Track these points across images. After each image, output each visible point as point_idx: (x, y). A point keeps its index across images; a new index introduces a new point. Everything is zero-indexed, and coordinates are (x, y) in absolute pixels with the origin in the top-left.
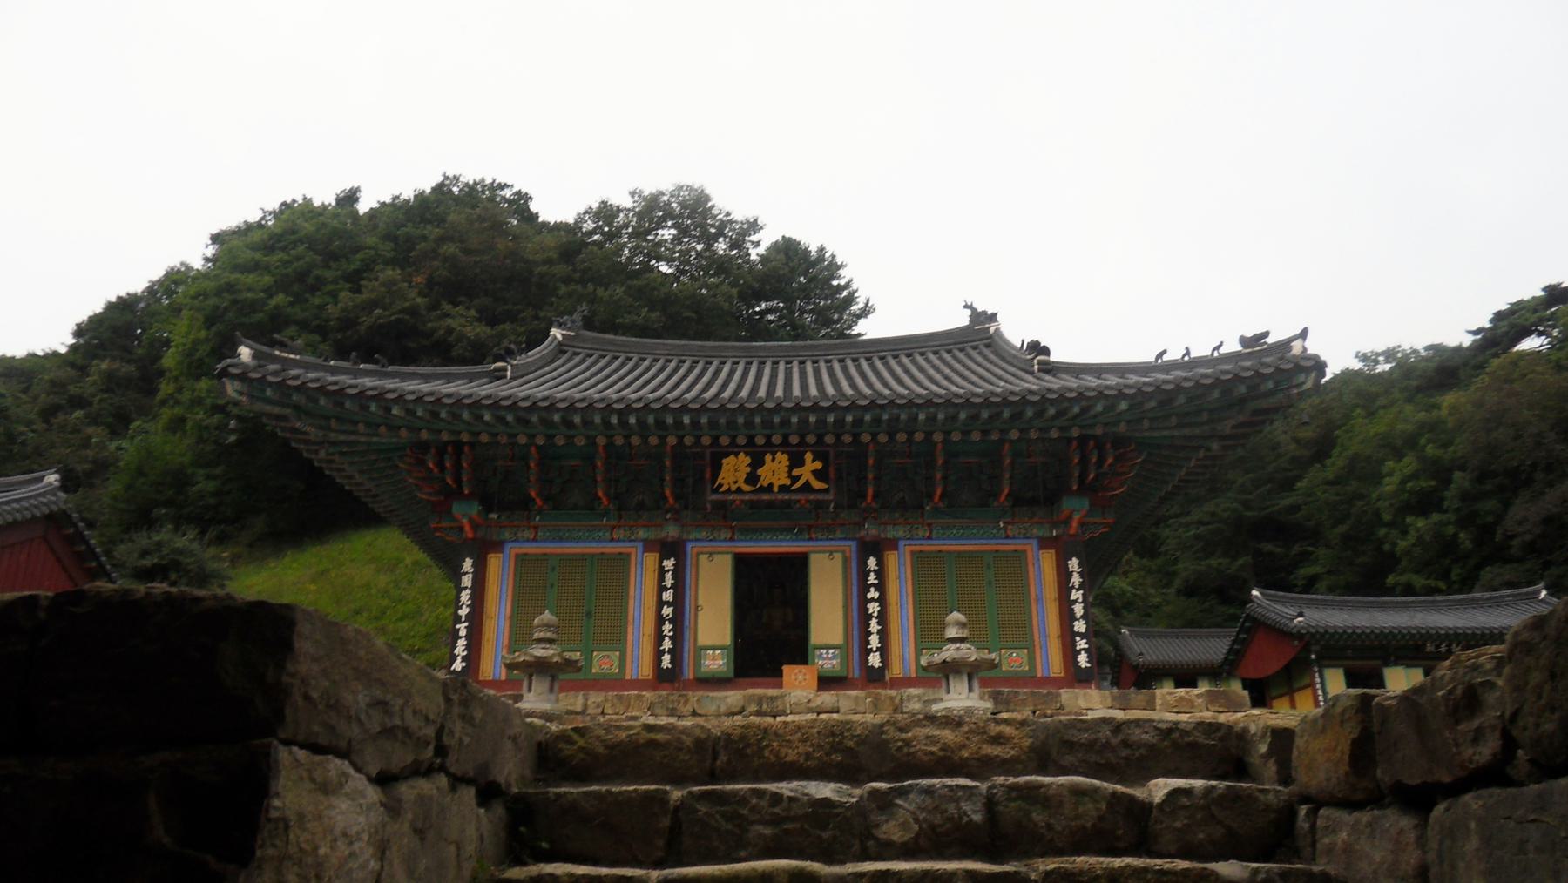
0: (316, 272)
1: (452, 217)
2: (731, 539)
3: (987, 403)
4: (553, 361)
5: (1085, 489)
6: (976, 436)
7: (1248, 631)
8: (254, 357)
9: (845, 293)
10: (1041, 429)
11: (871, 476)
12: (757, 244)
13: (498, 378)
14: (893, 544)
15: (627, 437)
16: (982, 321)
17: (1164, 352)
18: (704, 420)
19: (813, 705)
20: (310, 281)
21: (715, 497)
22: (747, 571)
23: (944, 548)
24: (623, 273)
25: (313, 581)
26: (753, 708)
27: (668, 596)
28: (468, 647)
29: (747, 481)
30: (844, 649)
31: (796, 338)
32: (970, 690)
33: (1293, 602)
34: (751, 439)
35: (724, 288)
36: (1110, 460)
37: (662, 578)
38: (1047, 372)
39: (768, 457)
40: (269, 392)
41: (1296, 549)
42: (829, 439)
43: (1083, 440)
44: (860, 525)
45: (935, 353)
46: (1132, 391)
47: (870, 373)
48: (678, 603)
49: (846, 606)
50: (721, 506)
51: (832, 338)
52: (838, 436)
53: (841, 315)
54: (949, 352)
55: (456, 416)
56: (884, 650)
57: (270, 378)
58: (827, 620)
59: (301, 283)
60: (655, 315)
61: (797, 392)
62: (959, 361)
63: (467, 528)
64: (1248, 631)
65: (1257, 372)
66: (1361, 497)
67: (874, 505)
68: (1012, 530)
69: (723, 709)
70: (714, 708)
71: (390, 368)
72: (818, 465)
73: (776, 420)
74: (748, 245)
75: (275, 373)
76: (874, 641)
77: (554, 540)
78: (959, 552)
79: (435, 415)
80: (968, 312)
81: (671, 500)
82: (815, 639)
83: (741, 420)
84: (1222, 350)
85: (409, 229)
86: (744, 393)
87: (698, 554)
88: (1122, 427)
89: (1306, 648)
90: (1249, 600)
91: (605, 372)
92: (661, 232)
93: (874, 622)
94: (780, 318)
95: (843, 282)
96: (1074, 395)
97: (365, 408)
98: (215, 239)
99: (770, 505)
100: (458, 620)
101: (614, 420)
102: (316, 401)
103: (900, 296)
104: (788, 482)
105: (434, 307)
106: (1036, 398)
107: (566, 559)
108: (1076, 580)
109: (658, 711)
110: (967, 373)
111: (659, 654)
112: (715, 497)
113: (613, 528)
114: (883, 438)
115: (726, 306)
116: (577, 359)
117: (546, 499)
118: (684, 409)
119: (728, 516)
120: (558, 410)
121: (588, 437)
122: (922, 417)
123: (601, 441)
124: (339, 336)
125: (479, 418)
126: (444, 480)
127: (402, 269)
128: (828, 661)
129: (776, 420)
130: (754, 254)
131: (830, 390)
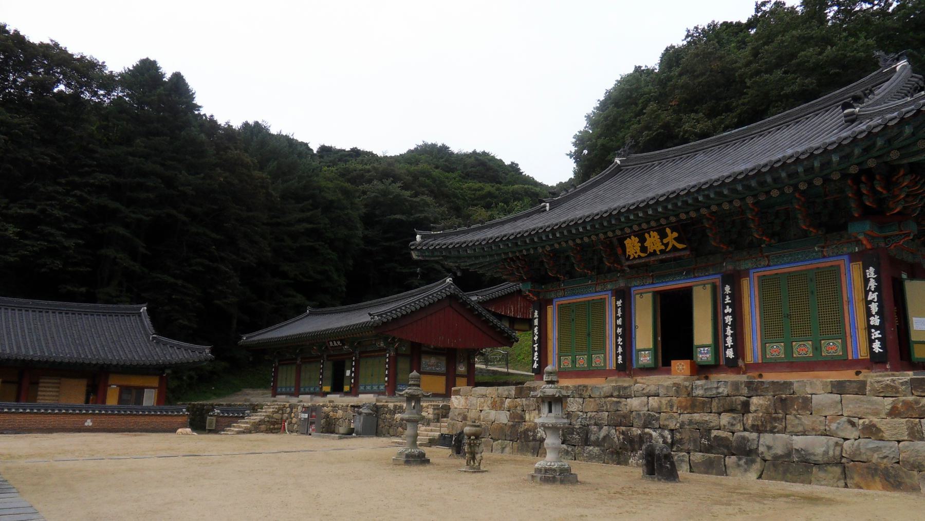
2: (653, 283)
5: (867, 213)
14: (746, 273)
21: (627, 263)
26: (615, 394)
27: (619, 322)
28: (539, 356)
32: (550, 411)
39: (647, 235)
72: (675, 235)
78: (789, 273)
82: (697, 341)
104: (663, 247)
112: (627, 263)
119: (647, 269)
127: (435, 197)
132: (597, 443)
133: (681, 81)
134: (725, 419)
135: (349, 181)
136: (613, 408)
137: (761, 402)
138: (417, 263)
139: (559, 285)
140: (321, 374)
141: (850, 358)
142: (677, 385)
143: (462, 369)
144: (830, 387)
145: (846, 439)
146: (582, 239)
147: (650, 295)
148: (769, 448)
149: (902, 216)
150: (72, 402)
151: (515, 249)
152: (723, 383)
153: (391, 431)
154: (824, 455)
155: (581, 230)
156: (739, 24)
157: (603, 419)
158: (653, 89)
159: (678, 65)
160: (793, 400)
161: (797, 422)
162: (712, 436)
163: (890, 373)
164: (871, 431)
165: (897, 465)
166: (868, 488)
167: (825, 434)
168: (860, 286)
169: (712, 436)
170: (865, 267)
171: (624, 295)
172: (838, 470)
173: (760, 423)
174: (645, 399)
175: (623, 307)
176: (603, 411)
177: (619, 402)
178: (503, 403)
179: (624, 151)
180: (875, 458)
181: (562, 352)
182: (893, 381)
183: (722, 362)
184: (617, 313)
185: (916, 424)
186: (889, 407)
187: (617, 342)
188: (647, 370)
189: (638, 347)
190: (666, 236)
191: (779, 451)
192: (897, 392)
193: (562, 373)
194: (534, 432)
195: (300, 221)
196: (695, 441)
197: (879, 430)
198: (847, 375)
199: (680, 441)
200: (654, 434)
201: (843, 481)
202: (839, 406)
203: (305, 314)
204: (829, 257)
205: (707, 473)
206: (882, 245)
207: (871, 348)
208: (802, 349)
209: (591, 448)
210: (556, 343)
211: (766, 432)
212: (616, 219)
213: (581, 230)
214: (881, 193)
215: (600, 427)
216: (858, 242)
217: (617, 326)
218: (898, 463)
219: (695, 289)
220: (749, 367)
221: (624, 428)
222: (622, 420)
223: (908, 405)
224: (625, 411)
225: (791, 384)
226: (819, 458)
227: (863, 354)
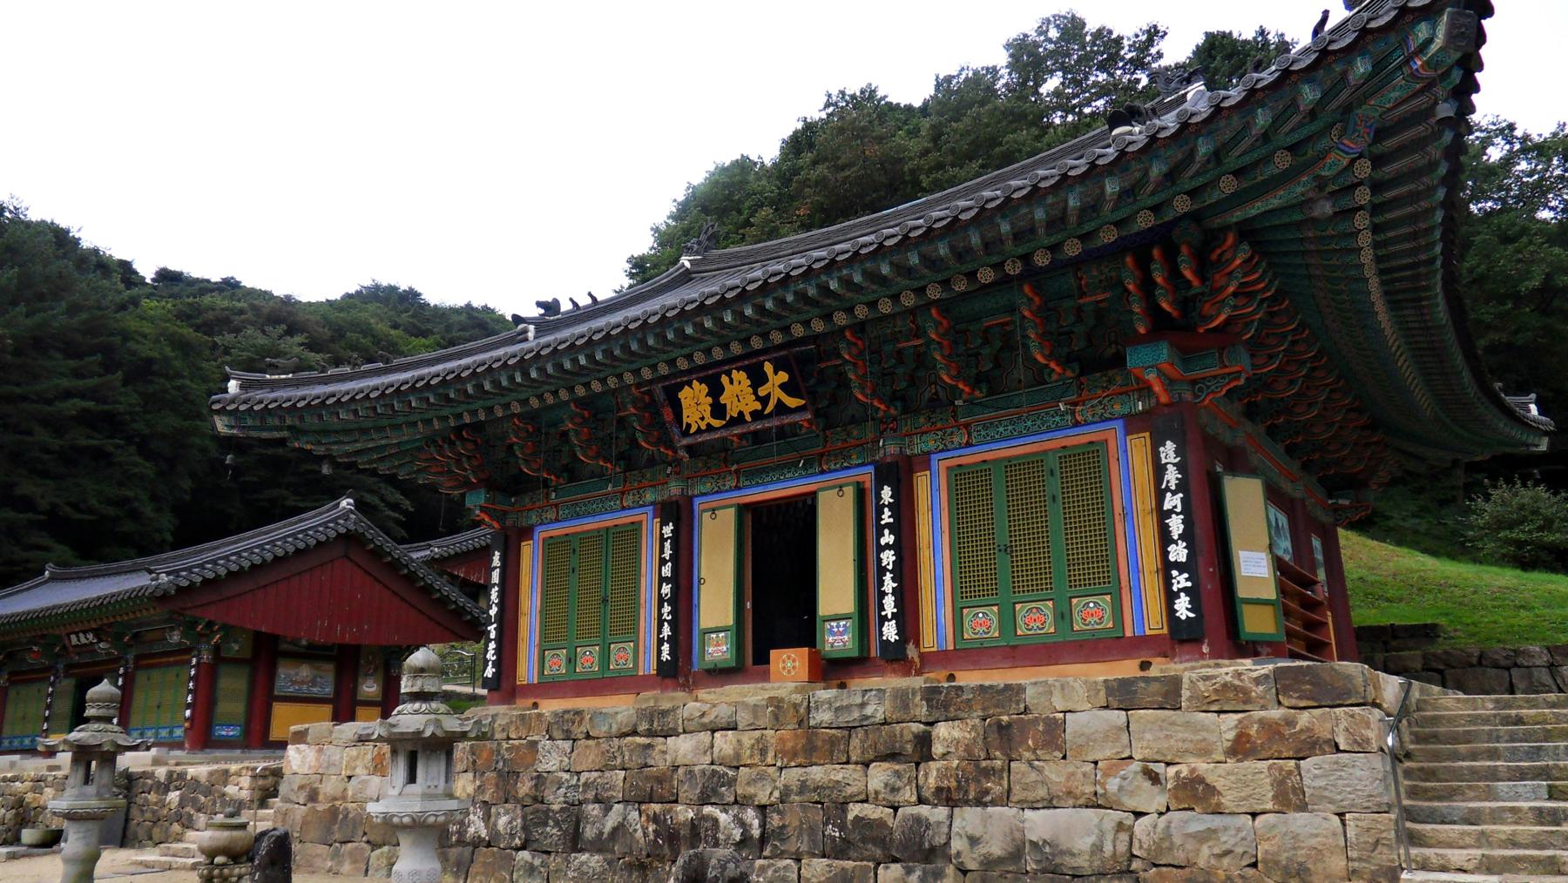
2: (737, 488)
5: (1161, 326)
14: (924, 461)
19: (706, 720)
21: (685, 442)
23: (556, 533)
26: (643, 727)
27: (667, 571)
28: (498, 651)
32: (412, 778)
39: (724, 379)
68: (1082, 412)
70: (604, 729)
72: (783, 377)
78: (1009, 459)
82: (823, 609)
104: (758, 406)
107: (585, 537)
109: (556, 734)
112: (685, 442)
117: (978, 381)
132: (598, 846)
133: (814, 175)
134: (879, 776)
135: (197, 328)
137: (956, 734)
138: (227, 443)
139: (547, 496)
140: (49, 707)
141: (1129, 633)
142: (776, 703)
143: (370, 688)
144: (1102, 694)
145: (1138, 815)
146: (587, 385)
147: (732, 511)
148: (974, 841)
149: (1225, 336)
151: (446, 412)
152: (873, 696)
153: (156, 832)
154: (1093, 853)
155: (583, 361)
156: (909, 108)
158: (771, 188)
159: (811, 146)
161: (1033, 776)
162: (850, 817)
163: (1212, 662)
164: (1195, 793)
165: (1251, 871)
167: (1095, 803)
168: (1144, 476)
169: (850, 817)
170: (1157, 444)
171: (679, 514)
173: (954, 784)
174: (705, 737)
175: (675, 539)
176: (614, 768)
177: (649, 746)
179: (699, 243)
180: (1204, 857)
181: (549, 639)
182: (1239, 675)
183: (875, 651)
184: (662, 551)
185: (1290, 773)
186: (1231, 735)
187: (660, 614)
188: (720, 674)
190: (764, 380)
191: (996, 849)
192: (1247, 701)
193: (548, 687)
194: (462, 823)
195: (68, 394)
196: (812, 830)
197: (1211, 790)
198: (1127, 669)
200: (723, 818)
202: (1125, 737)
203: (39, 580)
204: (1087, 424)
206: (1188, 396)
207: (1171, 611)
208: (1036, 619)
209: (584, 857)
211: (967, 803)
212: (656, 336)
213: (583, 361)
215: (606, 804)
216: (1145, 389)
217: (662, 580)
218: (1254, 865)
219: (821, 496)
220: (928, 660)
222: (652, 789)
223: (1272, 730)
225: (1021, 689)
227: (1155, 623)
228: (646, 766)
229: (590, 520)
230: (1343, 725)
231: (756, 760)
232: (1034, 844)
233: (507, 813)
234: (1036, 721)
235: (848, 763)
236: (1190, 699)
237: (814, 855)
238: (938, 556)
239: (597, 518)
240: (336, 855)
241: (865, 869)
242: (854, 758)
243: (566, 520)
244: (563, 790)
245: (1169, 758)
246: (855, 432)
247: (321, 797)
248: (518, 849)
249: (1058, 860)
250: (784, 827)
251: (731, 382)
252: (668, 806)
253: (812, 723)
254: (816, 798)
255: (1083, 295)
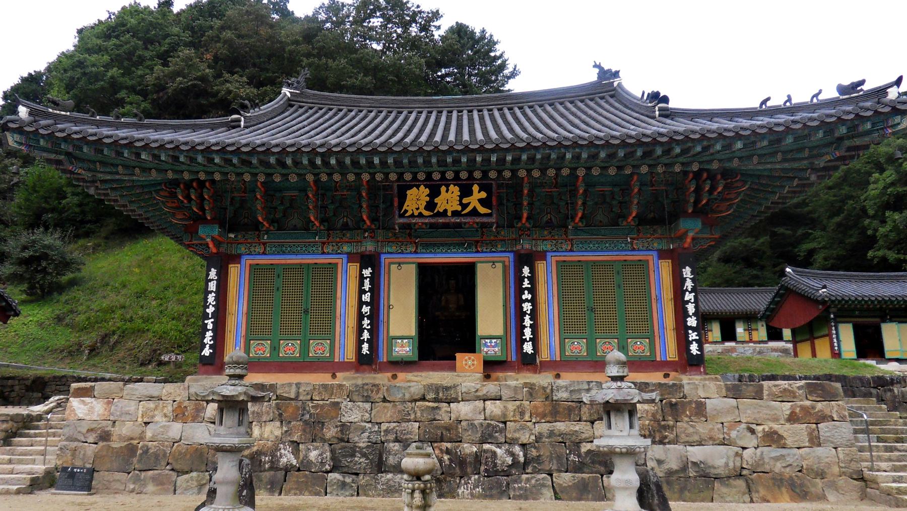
0: (139, 52)
1: (229, 13)
2: (416, 252)
3: (624, 144)
4: (283, 112)
5: (699, 212)
6: (612, 171)
7: (782, 296)
8: (30, 114)
9: (499, 62)
10: (666, 165)
11: (525, 203)
12: (439, 28)
13: (234, 127)
14: (542, 256)
15: (330, 175)
16: (607, 75)
17: (768, 99)
18: (390, 161)
19: (479, 394)
20: (135, 59)
21: (401, 220)
22: (428, 276)
24: (350, 48)
25: (139, 266)
26: (431, 396)
27: (366, 298)
28: (214, 338)
29: (426, 208)
30: (503, 339)
31: (466, 93)
32: (631, 427)
33: (815, 276)
34: (429, 176)
35: (416, 59)
36: (720, 189)
37: (362, 284)
38: (666, 116)
39: (443, 189)
40: (42, 142)
41: (800, 232)
42: (493, 175)
43: (697, 175)
44: (516, 240)
45: (571, 102)
46: (748, 133)
47: (523, 119)
48: (374, 304)
49: (505, 306)
50: (406, 227)
51: (491, 92)
52: (500, 172)
53: (497, 76)
54: (582, 101)
55: (193, 160)
56: (535, 340)
57: (41, 131)
58: (490, 317)
59: (128, 61)
60: (368, 79)
61: (466, 137)
62: (591, 109)
63: (211, 246)
64: (782, 296)
65: (857, 115)
66: (851, 197)
67: (528, 225)
68: (637, 244)
69: (407, 396)
71: (146, 121)
72: (483, 195)
73: (449, 160)
74: (433, 28)
75: (46, 127)
76: (528, 333)
77: (278, 254)
78: (594, 262)
79: (176, 159)
80: (597, 70)
81: (368, 222)
82: (482, 328)
83: (420, 160)
84: (821, 97)
85: (201, 22)
86: (423, 139)
87: (390, 264)
88: (735, 163)
89: (827, 311)
90: (783, 274)
91: (321, 121)
92: (372, 20)
93: (527, 318)
94: (455, 80)
95: (498, 54)
96: (697, 136)
97: (119, 154)
98: (80, 32)
99: (446, 226)
100: (206, 316)
101: (319, 161)
102: (81, 149)
103: (541, 60)
104: (459, 208)
105: (219, 75)
106: (665, 139)
107: (287, 268)
108: (689, 284)
109: (355, 398)
110: (600, 118)
111: (360, 343)
112: (401, 220)
113: (324, 243)
114: (536, 174)
115: (417, 71)
116: (301, 111)
117: (272, 222)
118: (374, 152)
119: (412, 235)
120: (274, 154)
121: (298, 175)
122: (569, 156)
123: (310, 178)
124: (155, 96)
125: (211, 160)
126: (190, 208)
127: (195, 48)
128: (491, 349)
129: (449, 160)
130: (437, 35)
131: (493, 134)
136: (427, 416)
144: (724, 390)
145: (744, 448)
148: (660, 462)
150: (646, 407)
157: (410, 433)
160: (684, 405)
161: (691, 430)
164: (773, 438)
166: (776, 500)
172: (741, 483)
174: (480, 404)
176: (409, 421)
178: (199, 410)
180: (778, 467)
186: (788, 412)
189: (392, 334)
191: (674, 465)
192: (795, 397)
194: (273, 455)
196: (559, 458)
197: (781, 437)
199: (538, 459)
200: (498, 451)
201: (747, 496)
202: (737, 411)
205: (580, 499)
209: (390, 476)
210: (243, 320)
214: (182, 202)
218: (800, 471)
221: (449, 445)
224: (447, 419)
226: (721, 471)
228: (435, 420)
229: (293, 257)
230: (835, 409)
231: (518, 418)
232: (694, 464)
233: (316, 448)
234: (690, 402)
235: (580, 421)
236: (768, 395)
237: (560, 471)
238: (551, 310)
239: (300, 257)
240: (137, 480)
241: (596, 479)
242: (584, 419)
243: (270, 254)
244: (366, 434)
245: (759, 422)
246: (659, 231)
247: (114, 438)
248: (327, 472)
249: (708, 471)
250: (539, 456)
251: (447, 191)
252: (457, 444)
253: (555, 398)
254: (561, 440)
255: (337, 190)
